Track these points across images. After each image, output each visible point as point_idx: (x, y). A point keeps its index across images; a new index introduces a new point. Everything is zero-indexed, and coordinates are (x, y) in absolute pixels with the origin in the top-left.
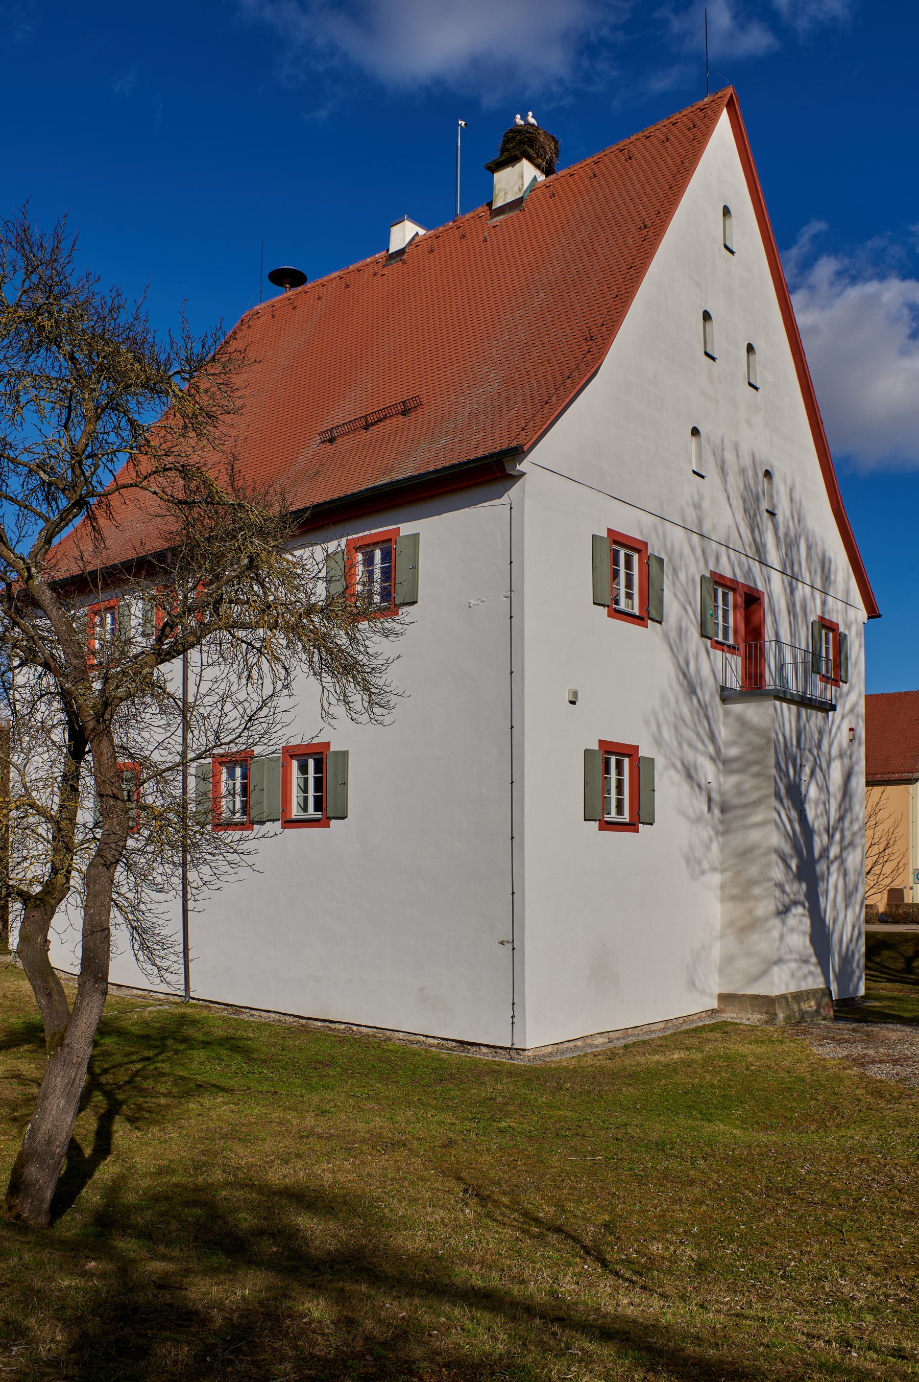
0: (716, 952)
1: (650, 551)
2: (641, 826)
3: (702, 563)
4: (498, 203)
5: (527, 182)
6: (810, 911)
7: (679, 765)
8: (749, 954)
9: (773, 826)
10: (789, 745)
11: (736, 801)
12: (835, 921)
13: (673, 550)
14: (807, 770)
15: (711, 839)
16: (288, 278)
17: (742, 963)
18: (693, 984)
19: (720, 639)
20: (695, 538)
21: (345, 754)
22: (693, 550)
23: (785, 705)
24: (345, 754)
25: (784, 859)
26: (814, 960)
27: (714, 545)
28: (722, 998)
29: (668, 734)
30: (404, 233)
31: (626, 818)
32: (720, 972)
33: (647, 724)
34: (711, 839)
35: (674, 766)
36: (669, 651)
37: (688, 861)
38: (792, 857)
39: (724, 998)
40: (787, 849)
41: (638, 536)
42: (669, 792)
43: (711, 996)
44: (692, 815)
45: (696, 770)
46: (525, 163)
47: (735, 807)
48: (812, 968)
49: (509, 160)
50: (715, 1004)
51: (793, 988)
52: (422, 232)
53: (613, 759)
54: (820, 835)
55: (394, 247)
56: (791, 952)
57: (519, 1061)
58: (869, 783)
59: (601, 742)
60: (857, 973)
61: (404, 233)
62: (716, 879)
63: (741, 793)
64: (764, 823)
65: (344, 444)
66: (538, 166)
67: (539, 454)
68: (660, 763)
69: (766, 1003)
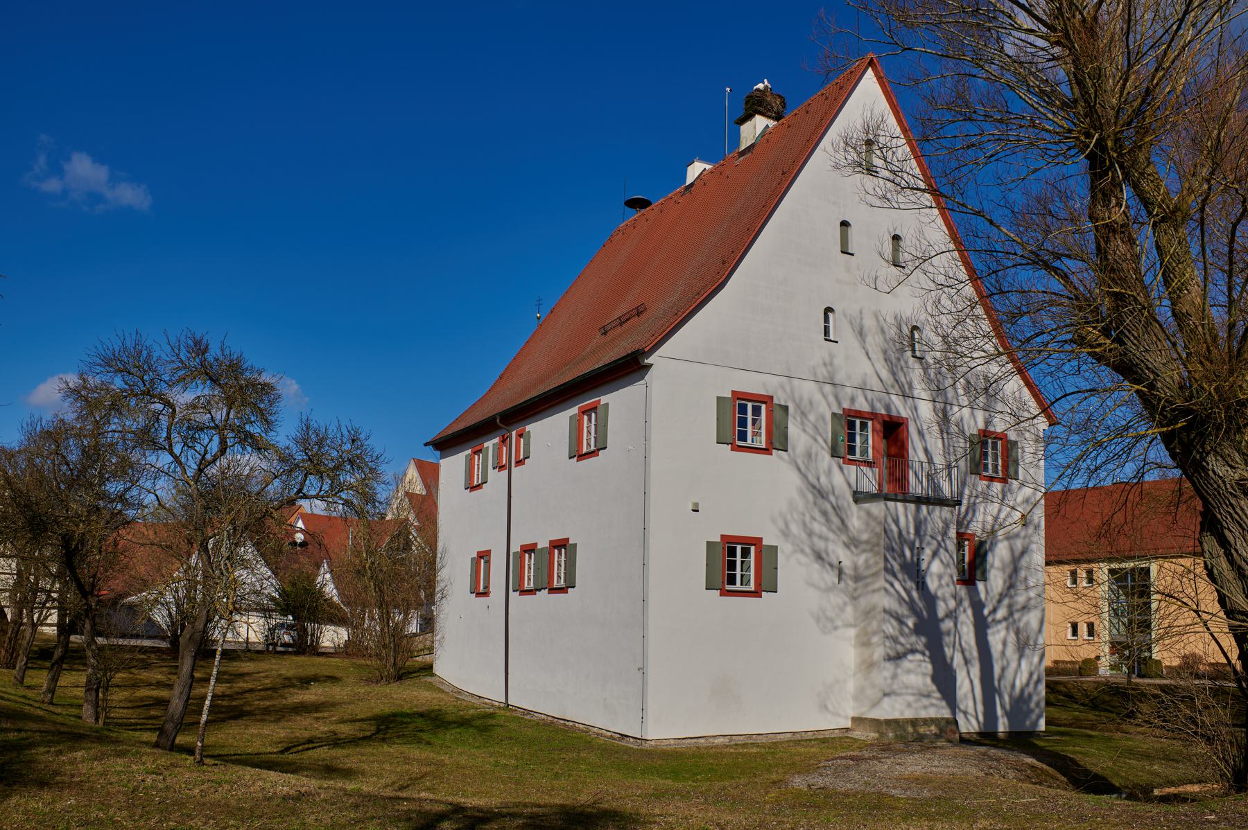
0: (851, 686)
1: (775, 401)
2: (764, 593)
4: (743, 147)
6: (930, 657)
7: (808, 550)
9: (883, 592)
10: (904, 533)
11: (866, 573)
12: (1003, 669)
13: (801, 399)
14: (928, 552)
15: (845, 604)
16: (639, 204)
18: (826, 707)
19: (999, 443)
21: (575, 545)
22: (825, 397)
23: (900, 505)
24: (575, 545)
26: (938, 695)
27: (849, 390)
28: (854, 719)
29: (795, 529)
30: (696, 169)
31: (752, 587)
33: (774, 521)
34: (845, 604)
35: (802, 551)
36: (796, 472)
37: (818, 620)
38: (908, 617)
40: (903, 610)
41: (763, 392)
42: (794, 569)
43: (846, 717)
44: (823, 585)
45: (827, 554)
46: (758, 117)
47: (866, 577)
49: (747, 117)
50: (849, 724)
51: (909, 714)
52: (708, 167)
53: (739, 548)
54: (945, 600)
55: (689, 181)
57: (646, 746)
58: (1052, 561)
60: (1037, 711)
61: (696, 169)
62: (852, 632)
63: (868, 567)
64: (878, 590)
65: (610, 335)
67: (662, 351)
69: (876, 723)
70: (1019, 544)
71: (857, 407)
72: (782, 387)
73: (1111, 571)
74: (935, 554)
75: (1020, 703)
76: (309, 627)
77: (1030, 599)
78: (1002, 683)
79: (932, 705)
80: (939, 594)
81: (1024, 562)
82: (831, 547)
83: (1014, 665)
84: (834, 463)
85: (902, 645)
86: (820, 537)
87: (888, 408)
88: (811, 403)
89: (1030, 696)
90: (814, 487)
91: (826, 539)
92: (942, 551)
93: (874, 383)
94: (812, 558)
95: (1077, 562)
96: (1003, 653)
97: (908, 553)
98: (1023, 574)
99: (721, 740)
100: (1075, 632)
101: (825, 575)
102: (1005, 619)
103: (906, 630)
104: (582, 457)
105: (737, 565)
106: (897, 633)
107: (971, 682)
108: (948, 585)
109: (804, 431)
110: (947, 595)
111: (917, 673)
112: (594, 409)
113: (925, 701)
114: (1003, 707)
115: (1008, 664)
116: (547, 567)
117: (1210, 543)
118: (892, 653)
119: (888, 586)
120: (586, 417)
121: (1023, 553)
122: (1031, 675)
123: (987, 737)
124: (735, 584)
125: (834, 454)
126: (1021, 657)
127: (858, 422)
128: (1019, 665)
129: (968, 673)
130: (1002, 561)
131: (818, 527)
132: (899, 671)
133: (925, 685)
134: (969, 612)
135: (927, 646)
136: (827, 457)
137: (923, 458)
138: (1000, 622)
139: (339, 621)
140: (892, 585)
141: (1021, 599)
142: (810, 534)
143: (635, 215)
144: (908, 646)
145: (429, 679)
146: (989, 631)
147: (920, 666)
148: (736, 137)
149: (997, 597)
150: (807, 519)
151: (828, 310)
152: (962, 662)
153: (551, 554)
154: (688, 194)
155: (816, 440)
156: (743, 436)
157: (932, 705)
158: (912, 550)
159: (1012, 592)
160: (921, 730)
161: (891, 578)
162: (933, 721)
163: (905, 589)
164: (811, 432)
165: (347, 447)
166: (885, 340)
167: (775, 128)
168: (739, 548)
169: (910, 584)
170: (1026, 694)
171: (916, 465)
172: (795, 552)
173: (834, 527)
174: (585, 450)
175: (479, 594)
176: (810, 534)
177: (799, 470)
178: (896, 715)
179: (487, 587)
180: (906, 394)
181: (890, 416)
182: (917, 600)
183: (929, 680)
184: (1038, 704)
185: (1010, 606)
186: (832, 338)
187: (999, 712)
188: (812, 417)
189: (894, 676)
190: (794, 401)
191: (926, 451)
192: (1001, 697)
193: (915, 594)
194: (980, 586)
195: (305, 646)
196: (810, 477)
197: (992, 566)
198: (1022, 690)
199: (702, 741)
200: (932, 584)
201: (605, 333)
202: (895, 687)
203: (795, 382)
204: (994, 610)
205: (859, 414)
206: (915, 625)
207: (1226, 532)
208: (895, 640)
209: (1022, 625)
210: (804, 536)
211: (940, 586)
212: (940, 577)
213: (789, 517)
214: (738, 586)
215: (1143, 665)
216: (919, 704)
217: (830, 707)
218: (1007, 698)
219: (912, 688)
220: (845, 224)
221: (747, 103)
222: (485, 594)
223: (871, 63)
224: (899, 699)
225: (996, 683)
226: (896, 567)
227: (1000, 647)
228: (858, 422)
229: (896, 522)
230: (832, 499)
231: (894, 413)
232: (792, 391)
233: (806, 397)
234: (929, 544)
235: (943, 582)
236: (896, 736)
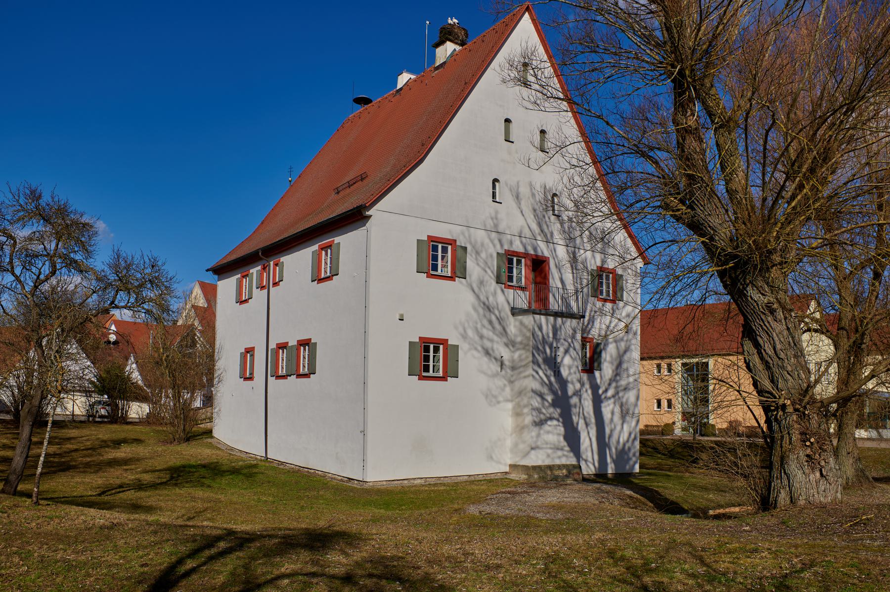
0: (509, 443)
1: (458, 243)
3: (498, 246)
4: (437, 64)
5: (449, 53)
6: (563, 423)
7: (480, 348)
8: (524, 442)
9: (531, 378)
15: (505, 385)
16: (363, 101)
17: (521, 446)
18: (492, 458)
20: (494, 235)
22: (492, 241)
23: (543, 318)
25: (541, 396)
26: (567, 448)
28: (511, 466)
30: (404, 78)
31: (441, 374)
32: (512, 451)
33: (456, 328)
34: (505, 385)
35: (476, 349)
36: (472, 293)
37: (487, 397)
39: (513, 467)
43: (505, 465)
44: (490, 373)
46: (448, 43)
48: (565, 453)
49: (441, 43)
50: (507, 469)
51: (548, 462)
52: (413, 77)
53: (432, 346)
54: (573, 383)
55: (399, 87)
56: (547, 443)
57: (366, 486)
59: (420, 338)
60: (634, 459)
61: (404, 78)
62: (510, 406)
63: (521, 360)
66: (456, 43)
67: (378, 206)
68: (464, 348)
69: (526, 468)
70: (623, 345)
72: (463, 234)
73: (684, 365)
74: (566, 351)
75: (622, 455)
76: (120, 403)
80: (569, 379)
82: (495, 346)
83: (619, 428)
87: (535, 249)
91: (492, 341)
92: (571, 349)
95: (662, 358)
96: (612, 420)
97: (548, 351)
100: (659, 406)
104: (321, 280)
106: (540, 406)
107: (590, 439)
109: (478, 264)
110: (575, 380)
111: (554, 433)
112: (329, 246)
113: (560, 453)
114: (611, 457)
116: (295, 360)
117: (748, 345)
118: (537, 420)
119: (534, 374)
120: (323, 252)
122: (630, 434)
123: (601, 477)
127: (440, 246)
128: (622, 427)
132: (542, 432)
133: (559, 442)
134: (590, 392)
135: (561, 415)
136: (494, 283)
138: (610, 398)
139: (141, 398)
140: (537, 373)
142: (481, 337)
143: (360, 109)
145: (209, 440)
148: (433, 57)
150: (479, 326)
151: (495, 181)
153: (298, 350)
154: (398, 96)
156: (435, 268)
159: (618, 378)
161: (536, 368)
164: (482, 265)
165: (148, 271)
167: (460, 51)
168: (432, 346)
169: (549, 372)
171: (554, 290)
172: (470, 349)
174: (323, 276)
175: (246, 379)
176: (481, 337)
177: (473, 291)
179: (252, 373)
181: (536, 256)
183: (562, 438)
184: (634, 455)
185: (617, 387)
186: (497, 200)
188: (483, 255)
190: (471, 243)
192: (610, 449)
194: (597, 374)
195: (117, 417)
197: (605, 360)
198: (624, 445)
200: (564, 372)
201: (338, 193)
202: (539, 443)
204: (606, 391)
207: (759, 338)
210: (477, 338)
211: (570, 374)
212: (570, 367)
213: (466, 325)
214: (431, 373)
215: (704, 428)
216: (555, 455)
217: (494, 457)
218: (614, 450)
220: (507, 121)
221: (441, 32)
222: (251, 378)
223: (528, 9)
224: (541, 452)
226: (540, 360)
228: (440, 246)
232: (470, 236)
236: (540, 477)
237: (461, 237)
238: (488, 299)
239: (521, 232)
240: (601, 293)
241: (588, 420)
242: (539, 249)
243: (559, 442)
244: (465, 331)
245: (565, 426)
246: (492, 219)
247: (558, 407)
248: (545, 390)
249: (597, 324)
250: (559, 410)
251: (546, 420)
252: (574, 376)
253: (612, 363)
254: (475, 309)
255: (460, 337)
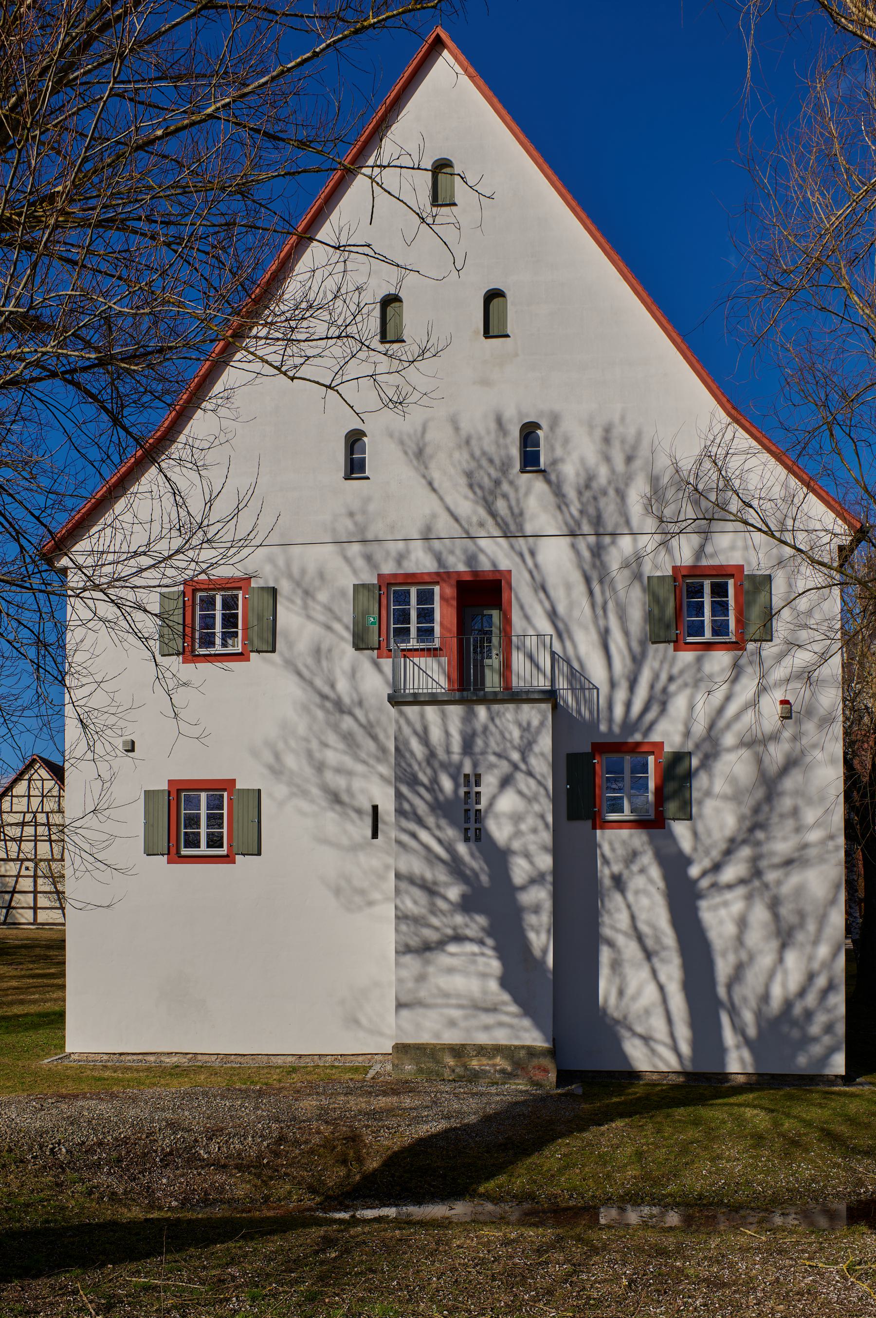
6: (495, 949)
7: (315, 791)
12: (739, 970)
13: (303, 572)
18: (357, 1022)
25: (430, 890)
26: (514, 1008)
33: (255, 754)
35: (305, 794)
36: (295, 678)
37: (338, 892)
38: (447, 885)
42: (289, 822)
44: (345, 841)
51: (451, 1037)
54: (527, 856)
70: (777, 753)
71: (410, 567)
74: (506, 782)
75: (780, 1027)
77: (805, 846)
78: (738, 992)
79: (501, 1024)
80: (516, 845)
81: (789, 783)
82: (357, 784)
83: (766, 960)
84: (364, 659)
85: (437, 929)
86: (339, 770)
87: (471, 559)
88: (321, 575)
89: (809, 1015)
90: (324, 697)
91: (350, 773)
92: (520, 777)
93: (444, 525)
94: (324, 804)
96: (740, 940)
97: (447, 784)
98: (787, 803)
99: (290, 1059)
101: (350, 827)
102: (742, 881)
103: (441, 904)
105: (199, 822)
106: (424, 911)
107: (661, 988)
108: (535, 831)
109: (309, 617)
110: (532, 848)
113: (488, 1019)
114: (739, 1029)
115: (751, 958)
118: (414, 942)
119: (405, 838)
121: (791, 764)
122: (811, 977)
124: (198, 846)
125: (360, 643)
126: (783, 946)
128: (781, 960)
129: (654, 973)
130: (732, 780)
131: (332, 757)
132: (431, 969)
133: (485, 992)
134: (655, 872)
135: (490, 931)
136: (350, 650)
137: (544, 626)
138: (730, 887)
140: (414, 836)
141: (781, 845)
142: (320, 767)
144: (449, 932)
146: (703, 904)
147: (474, 962)
149: (723, 846)
150: (315, 745)
152: (640, 955)
155: (329, 628)
157: (501, 1024)
158: (454, 778)
159: (760, 835)
160: (475, 1063)
161: (412, 826)
162: (498, 1049)
163: (440, 841)
164: (321, 618)
166: (472, 456)
169: (451, 833)
170: (797, 1010)
171: (531, 643)
172: (293, 795)
173: (363, 755)
176: (320, 767)
177: (299, 674)
178: (425, 1038)
180: (511, 530)
181: (475, 573)
182: (467, 858)
183: (493, 985)
184: (829, 1028)
185: (755, 860)
187: (729, 1037)
188: (323, 596)
189: (421, 978)
190: (290, 576)
191: (553, 615)
192: (734, 1012)
193: (462, 849)
194: (681, 830)
196: (319, 682)
197: (708, 793)
198: (788, 1004)
199: (152, 1058)
200: (499, 831)
202: (422, 994)
203: (296, 550)
204: (717, 867)
205: (411, 579)
206: (464, 896)
208: (417, 921)
209: (786, 889)
210: (309, 771)
211: (518, 834)
212: (517, 818)
213: (281, 746)
216: (474, 1022)
217: (364, 1021)
218: (748, 1016)
219: (458, 996)
224: (432, 1014)
225: (722, 991)
226: (422, 808)
227: (730, 929)
229: (425, 740)
230: (358, 713)
231: (485, 565)
232: (288, 565)
233: (312, 569)
234: (492, 766)
235: (523, 827)
236: (420, 1071)
237: (268, 569)
238: (333, 686)
239: (429, 529)
240: (698, 630)
241: (650, 943)
242: (482, 558)
243: (485, 992)
244: (277, 756)
245: (501, 952)
246: (351, 515)
247: (480, 912)
248: (441, 875)
249: (679, 704)
250: (482, 920)
251: (441, 945)
252: (531, 837)
253: (736, 797)
254: (306, 709)
255: (266, 772)
